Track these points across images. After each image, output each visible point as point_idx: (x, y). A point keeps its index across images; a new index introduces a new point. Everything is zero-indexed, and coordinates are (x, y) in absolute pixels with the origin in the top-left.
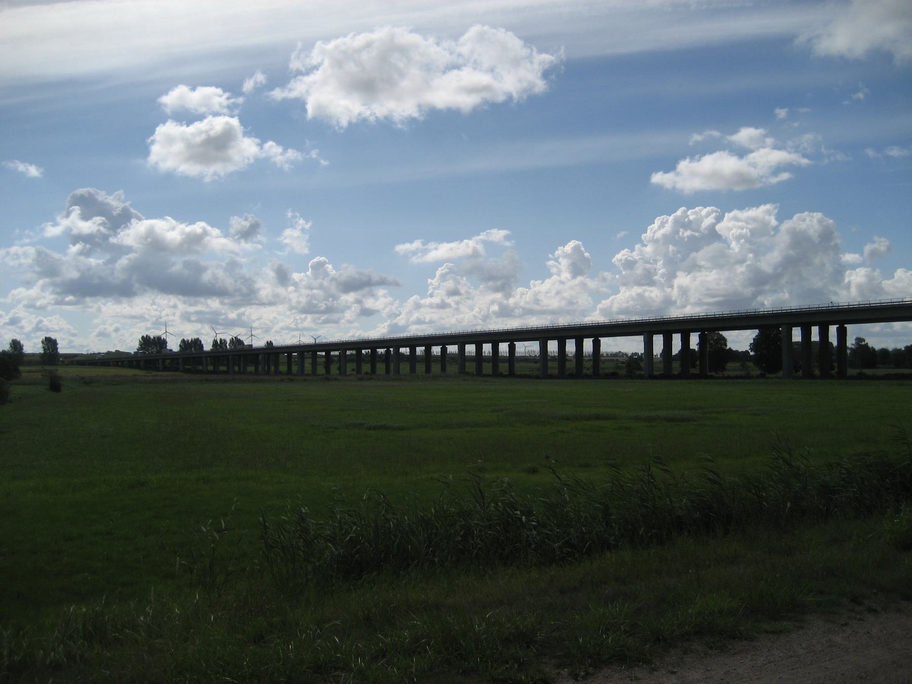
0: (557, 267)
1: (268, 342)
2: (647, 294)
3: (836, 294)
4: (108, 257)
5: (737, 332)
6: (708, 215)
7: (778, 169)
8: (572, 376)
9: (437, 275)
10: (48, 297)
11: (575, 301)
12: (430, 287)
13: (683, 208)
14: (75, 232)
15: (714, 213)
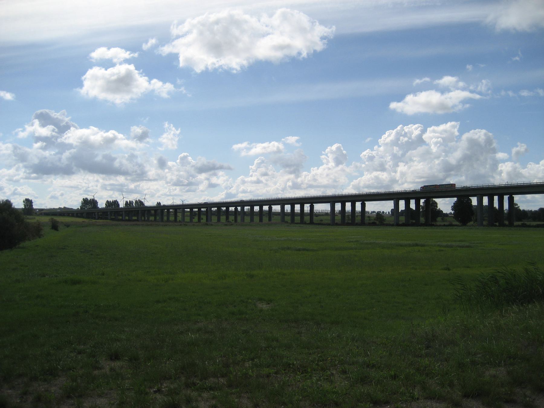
0: (326, 159)
1: (158, 203)
2: (380, 176)
3: (493, 177)
4: (57, 151)
5: (449, 199)
6: (416, 129)
7: (464, 101)
8: (348, 224)
9: (255, 163)
10: (22, 173)
11: (337, 180)
12: (251, 171)
13: (401, 126)
14: (37, 135)
15: (420, 128)
